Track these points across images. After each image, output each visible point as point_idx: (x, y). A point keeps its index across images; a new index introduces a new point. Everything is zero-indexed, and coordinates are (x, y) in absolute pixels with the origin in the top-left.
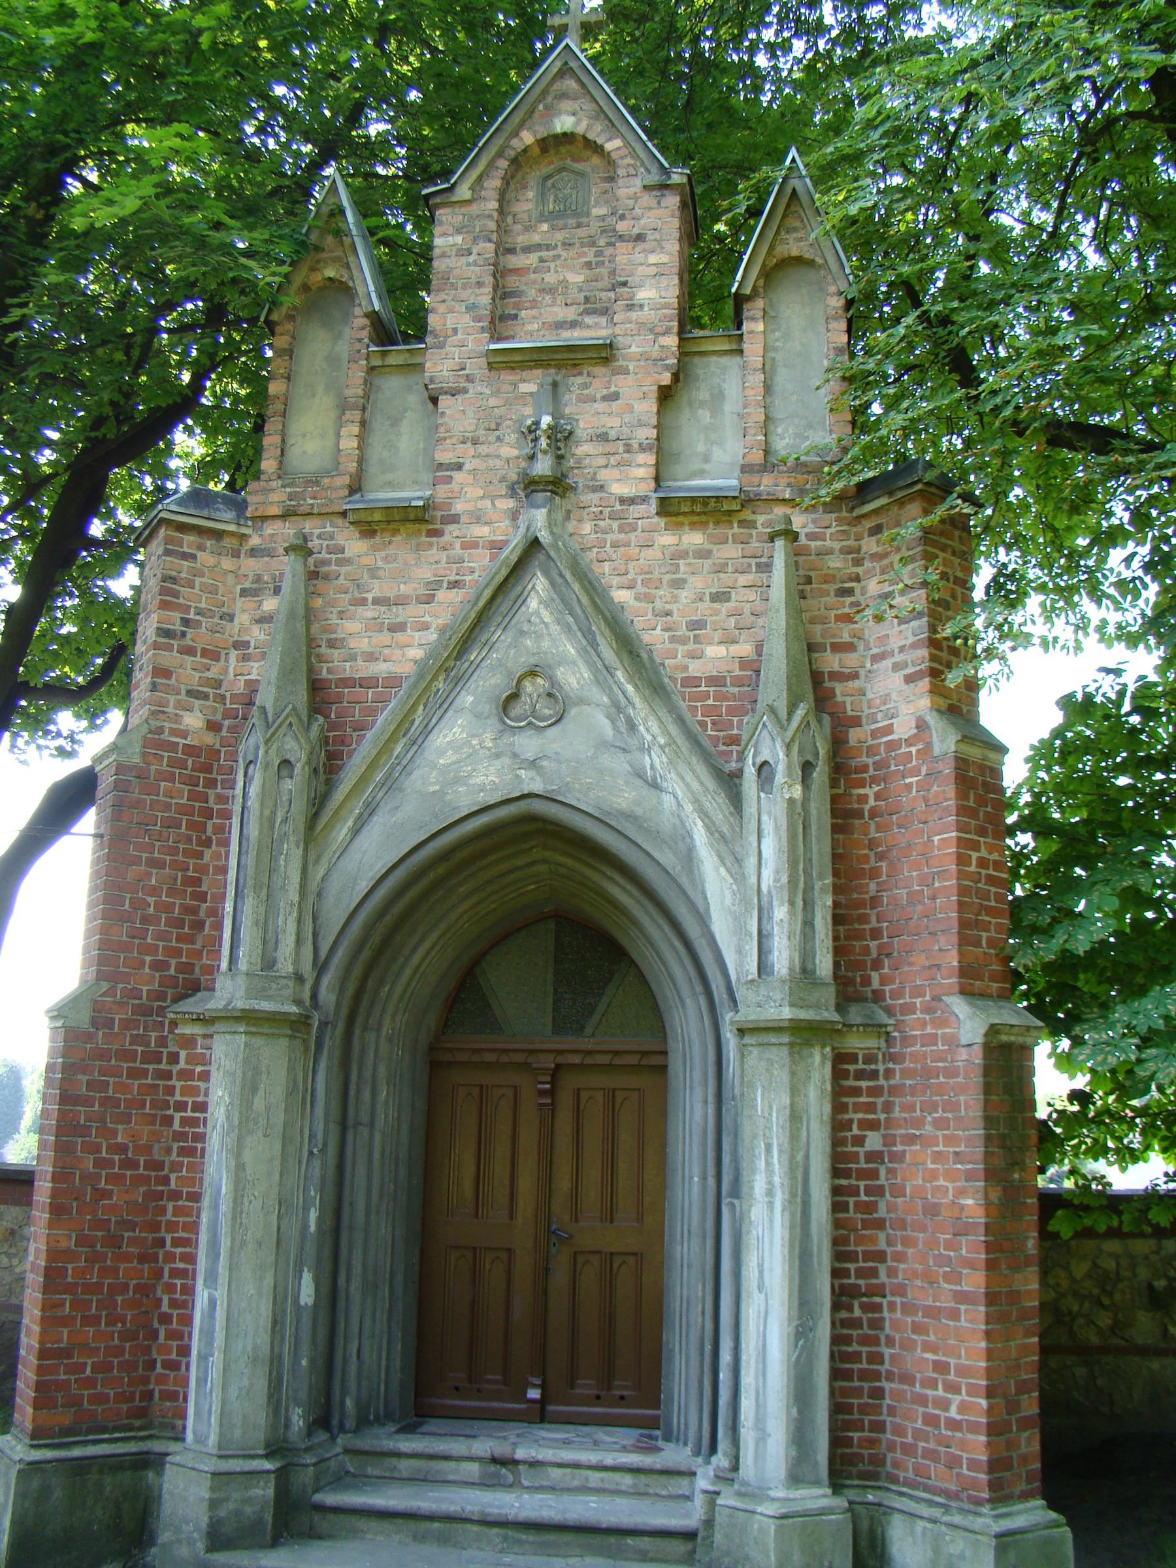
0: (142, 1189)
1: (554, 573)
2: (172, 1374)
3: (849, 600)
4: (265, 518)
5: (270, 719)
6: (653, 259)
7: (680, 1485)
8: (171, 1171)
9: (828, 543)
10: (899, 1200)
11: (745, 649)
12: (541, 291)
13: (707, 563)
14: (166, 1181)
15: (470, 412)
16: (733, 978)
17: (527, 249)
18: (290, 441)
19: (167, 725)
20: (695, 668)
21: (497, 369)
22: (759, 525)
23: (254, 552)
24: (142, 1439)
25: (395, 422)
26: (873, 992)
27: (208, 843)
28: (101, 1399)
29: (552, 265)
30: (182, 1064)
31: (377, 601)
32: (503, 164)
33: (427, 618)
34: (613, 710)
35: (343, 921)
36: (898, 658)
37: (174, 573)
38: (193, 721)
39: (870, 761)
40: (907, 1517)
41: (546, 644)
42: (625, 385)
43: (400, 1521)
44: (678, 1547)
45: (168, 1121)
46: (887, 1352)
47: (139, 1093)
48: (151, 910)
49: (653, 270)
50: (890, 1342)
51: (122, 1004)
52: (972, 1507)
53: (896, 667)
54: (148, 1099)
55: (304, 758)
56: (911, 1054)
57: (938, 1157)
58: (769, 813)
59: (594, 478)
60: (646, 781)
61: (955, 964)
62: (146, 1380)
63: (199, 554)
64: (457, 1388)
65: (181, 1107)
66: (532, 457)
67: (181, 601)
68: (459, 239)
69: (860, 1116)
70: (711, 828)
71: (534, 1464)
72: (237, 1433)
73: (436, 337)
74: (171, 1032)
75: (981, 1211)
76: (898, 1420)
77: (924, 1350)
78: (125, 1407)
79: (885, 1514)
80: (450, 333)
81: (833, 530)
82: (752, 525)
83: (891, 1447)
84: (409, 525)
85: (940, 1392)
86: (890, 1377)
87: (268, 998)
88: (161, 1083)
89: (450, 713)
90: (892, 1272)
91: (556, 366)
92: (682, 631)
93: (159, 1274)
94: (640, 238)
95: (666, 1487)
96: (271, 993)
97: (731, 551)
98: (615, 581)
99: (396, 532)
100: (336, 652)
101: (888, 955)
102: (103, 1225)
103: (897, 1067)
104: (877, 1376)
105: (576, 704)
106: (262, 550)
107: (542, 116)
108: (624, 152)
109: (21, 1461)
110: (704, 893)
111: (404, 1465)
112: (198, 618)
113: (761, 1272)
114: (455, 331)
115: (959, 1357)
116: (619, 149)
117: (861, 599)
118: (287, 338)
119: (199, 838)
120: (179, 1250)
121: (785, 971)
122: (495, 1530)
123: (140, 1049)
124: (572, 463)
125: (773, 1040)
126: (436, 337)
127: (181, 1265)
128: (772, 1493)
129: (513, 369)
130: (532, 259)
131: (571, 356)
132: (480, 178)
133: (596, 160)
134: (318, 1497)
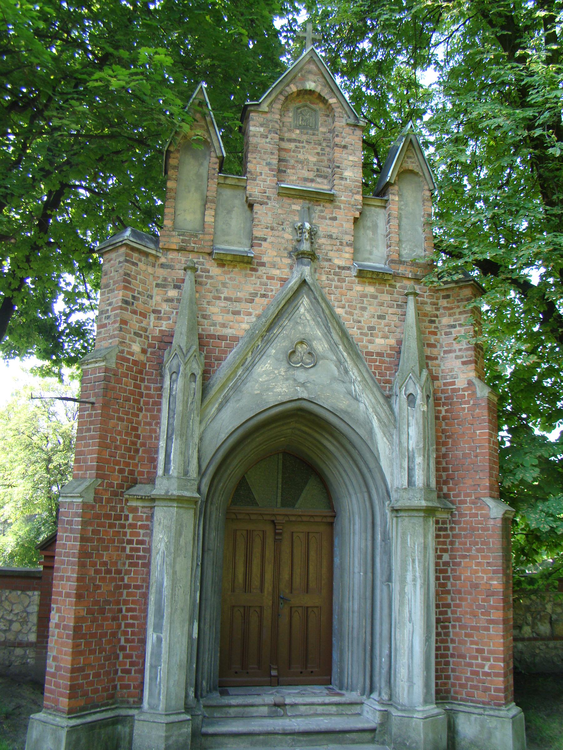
0: (113, 584)
1: (312, 297)
2: (127, 676)
3: (434, 325)
4: (168, 250)
5: (184, 351)
6: (351, 158)
7: (357, 709)
8: (126, 574)
9: (425, 299)
10: (457, 582)
11: (392, 341)
12: (297, 162)
13: (375, 301)
14: (122, 579)
15: (270, 214)
16: (390, 486)
17: (290, 140)
18: (178, 213)
19: (126, 349)
20: (371, 348)
21: (282, 196)
22: (397, 287)
23: (162, 266)
24: (113, 709)
25: (229, 212)
26: (444, 494)
27: (140, 410)
28: (96, 691)
29: (302, 151)
30: (130, 521)
31: (226, 299)
32: (282, 98)
33: (251, 310)
34: (338, 363)
35: (213, 453)
36: (458, 353)
37: (129, 272)
38: (136, 348)
39: (443, 396)
40: (466, 714)
41: (308, 329)
42: (340, 214)
43: (244, 737)
44: (368, 736)
45: (124, 549)
46: (451, 646)
47: (113, 536)
48: (118, 443)
49: (351, 163)
50: (453, 641)
51: (106, 490)
52: (496, 707)
53: (457, 357)
54: (116, 538)
55: (200, 373)
56: (464, 521)
57: (478, 564)
58: (413, 416)
59: (326, 255)
60: (352, 396)
61: (488, 484)
62: (114, 680)
63: (139, 263)
64: (236, 673)
65: (130, 542)
66: (299, 241)
67: (132, 286)
68: (262, 130)
69: (440, 546)
70: (379, 420)
71: (293, 705)
72: (173, 703)
73: (252, 174)
74: (126, 504)
75: (501, 586)
76: (457, 674)
77: (471, 644)
78: (105, 694)
79: (454, 713)
80: (258, 174)
81: (427, 294)
82: (394, 286)
83: (454, 685)
84: (242, 264)
85: (480, 661)
86: (453, 656)
87: (187, 490)
88: (121, 530)
89: (264, 357)
90: (454, 612)
91: (308, 200)
92: (366, 330)
93: (119, 626)
94: (345, 147)
95: (350, 710)
96: (188, 487)
97: (386, 298)
98: (336, 304)
99: (235, 267)
100: (206, 321)
101: (452, 479)
102: (96, 603)
103: (457, 526)
104: (446, 656)
105: (322, 359)
106: (167, 265)
107: (300, 79)
108: (337, 105)
109: (67, 726)
110: (377, 448)
111: (232, 711)
112: (138, 296)
113: (410, 614)
114: (261, 173)
115: (490, 646)
116: (335, 103)
117: (439, 326)
118: (176, 160)
119: (138, 407)
120: (130, 614)
121: (421, 485)
122: (289, 737)
123: (113, 513)
124: (316, 246)
125: (416, 515)
126: (252, 174)
127: (131, 621)
128: (418, 709)
129: (289, 197)
130: (292, 146)
131: (317, 196)
132: (271, 103)
133: (321, 105)
134: (204, 730)
